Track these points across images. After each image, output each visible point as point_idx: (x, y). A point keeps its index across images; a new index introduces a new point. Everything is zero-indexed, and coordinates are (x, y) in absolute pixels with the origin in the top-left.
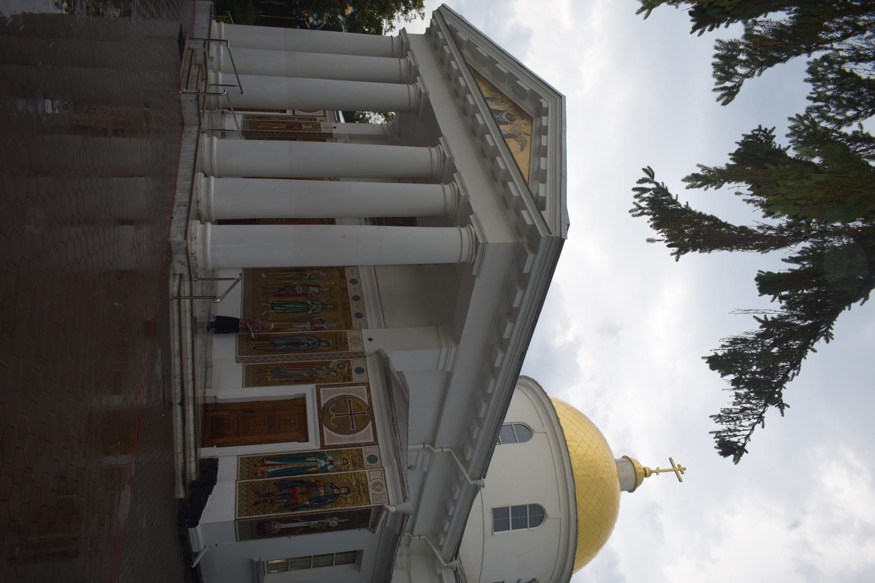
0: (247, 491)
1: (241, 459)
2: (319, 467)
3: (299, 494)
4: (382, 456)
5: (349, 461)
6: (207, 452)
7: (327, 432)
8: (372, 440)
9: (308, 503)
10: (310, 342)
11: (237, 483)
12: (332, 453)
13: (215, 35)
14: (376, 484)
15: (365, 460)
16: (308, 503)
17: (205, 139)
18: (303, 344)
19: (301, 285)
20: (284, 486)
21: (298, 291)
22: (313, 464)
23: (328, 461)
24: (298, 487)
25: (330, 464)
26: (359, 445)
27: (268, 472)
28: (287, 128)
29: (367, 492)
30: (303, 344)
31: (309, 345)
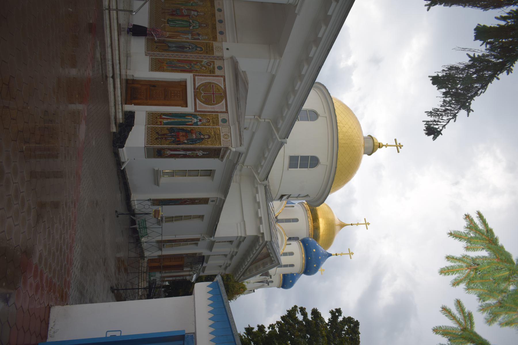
0: (151, 132)
1: (148, 113)
2: (193, 122)
6: (129, 108)
7: (198, 102)
9: (186, 141)
10: (190, 47)
12: (201, 115)
14: (225, 135)
16: (186, 141)
18: (186, 48)
19: (186, 10)
22: (190, 120)
23: (198, 119)
25: (199, 121)
26: (217, 112)
27: (163, 122)
30: (186, 48)
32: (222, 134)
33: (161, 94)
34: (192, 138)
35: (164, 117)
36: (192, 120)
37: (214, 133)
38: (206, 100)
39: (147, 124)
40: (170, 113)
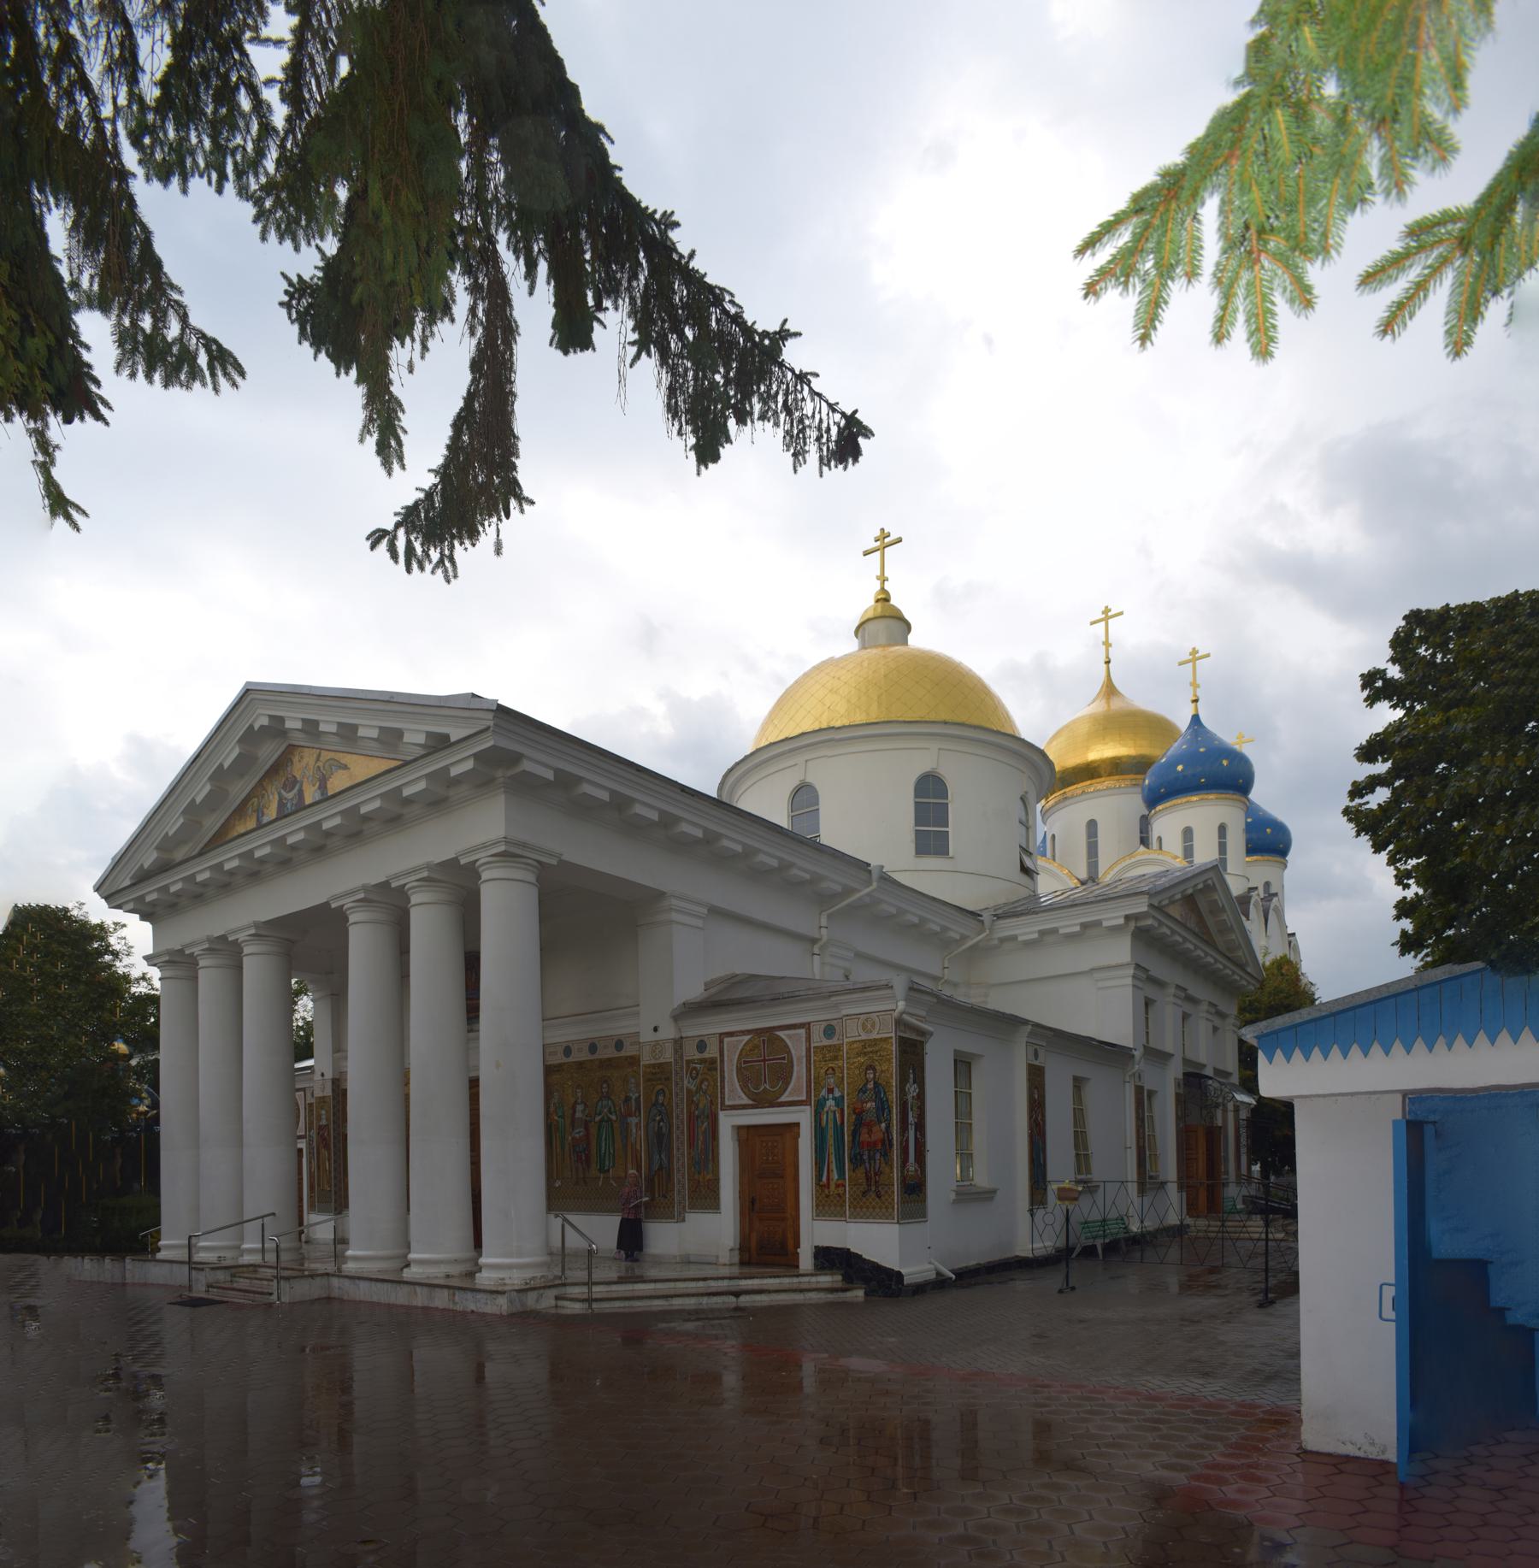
0: (861, 1208)
1: (817, 1216)
6: (806, 1261)
9: (883, 1125)
10: (658, 1118)
12: (818, 1090)
14: (864, 1028)
22: (831, 1115)
26: (808, 1050)
28: (327, 1147)
30: (660, 1128)
31: (662, 1120)
32: (864, 1037)
35: (824, 1179)
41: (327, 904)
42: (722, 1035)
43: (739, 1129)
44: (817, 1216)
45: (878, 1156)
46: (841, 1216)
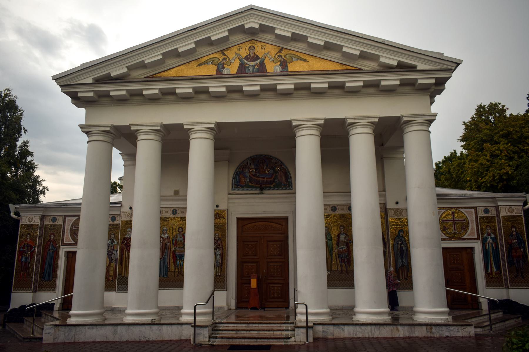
0: (515, 282)
1: (487, 286)
2: (492, 242)
3: (517, 254)
4: (486, 205)
5: (488, 224)
6: (485, 306)
8: (473, 210)
9: (522, 249)
10: (400, 243)
11: (510, 288)
12: (483, 234)
13: (190, 319)
14: (509, 211)
15: (53, 224)
16: (522, 249)
17: (72, 321)
18: (401, 247)
19: (338, 247)
20: (512, 262)
21: (344, 249)
22: (490, 245)
24: (512, 254)
25: (490, 236)
26: (476, 218)
27: (496, 271)
29: (514, 217)
30: (401, 247)
31: (402, 244)
32: (509, 214)
33: (457, 274)
34: (517, 243)
35: (489, 271)
36: (489, 243)
37: (508, 222)
38: (463, 228)
39: (115, 291)
40: (485, 264)
41: (129, 127)
42: (65, 216)
43: (472, 249)
44: (487, 286)
45: (521, 262)
46: (114, 290)
